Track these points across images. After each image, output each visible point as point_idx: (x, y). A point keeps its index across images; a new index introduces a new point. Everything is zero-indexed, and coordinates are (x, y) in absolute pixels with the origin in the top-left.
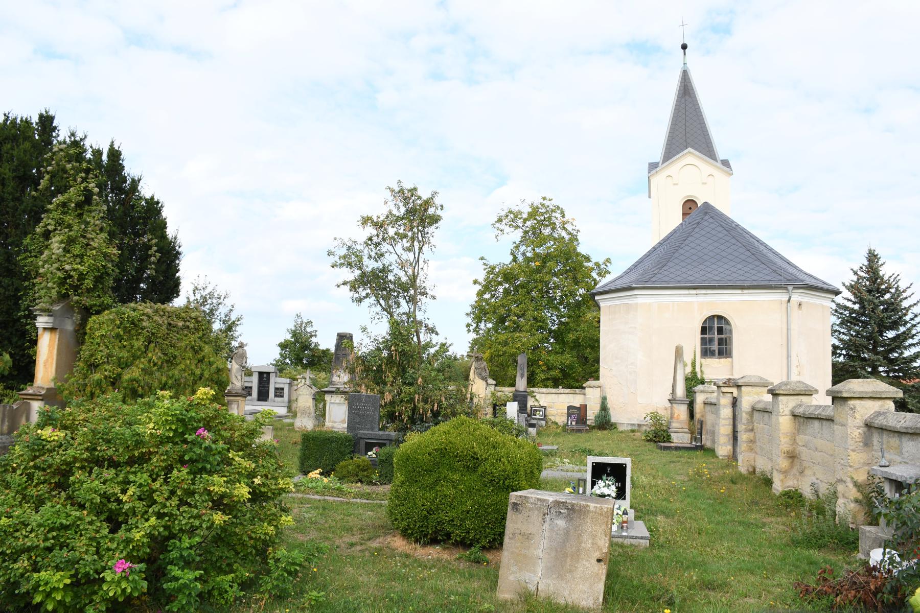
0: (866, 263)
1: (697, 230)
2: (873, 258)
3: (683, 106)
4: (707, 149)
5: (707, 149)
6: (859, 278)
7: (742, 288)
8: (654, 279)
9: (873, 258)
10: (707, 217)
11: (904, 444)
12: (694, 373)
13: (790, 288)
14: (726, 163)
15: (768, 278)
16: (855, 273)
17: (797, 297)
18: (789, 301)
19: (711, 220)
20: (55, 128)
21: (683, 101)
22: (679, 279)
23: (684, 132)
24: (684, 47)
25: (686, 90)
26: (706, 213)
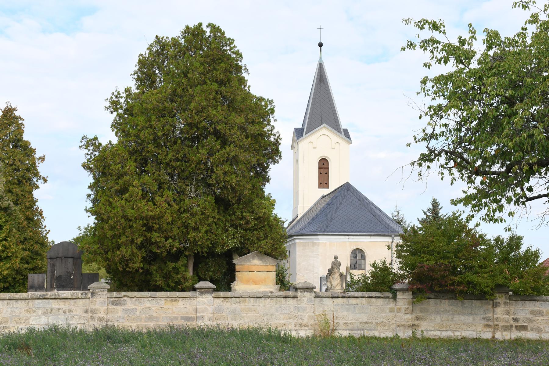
0: (431, 207)
1: (345, 200)
3: (319, 90)
4: (335, 125)
5: (334, 124)
6: (427, 216)
7: (371, 235)
8: (327, 230)
9: (435, 204)
10: (349, 192)
13: (393, 236)
14: (346, 133)
15: (383, 230)
16: (425, 213)
19: (351, 194)
21: (319, 86)
22: (340, 230)
23: (320, 111)
24: (321, 45)
25: (321, 79)
26: (348, 189)
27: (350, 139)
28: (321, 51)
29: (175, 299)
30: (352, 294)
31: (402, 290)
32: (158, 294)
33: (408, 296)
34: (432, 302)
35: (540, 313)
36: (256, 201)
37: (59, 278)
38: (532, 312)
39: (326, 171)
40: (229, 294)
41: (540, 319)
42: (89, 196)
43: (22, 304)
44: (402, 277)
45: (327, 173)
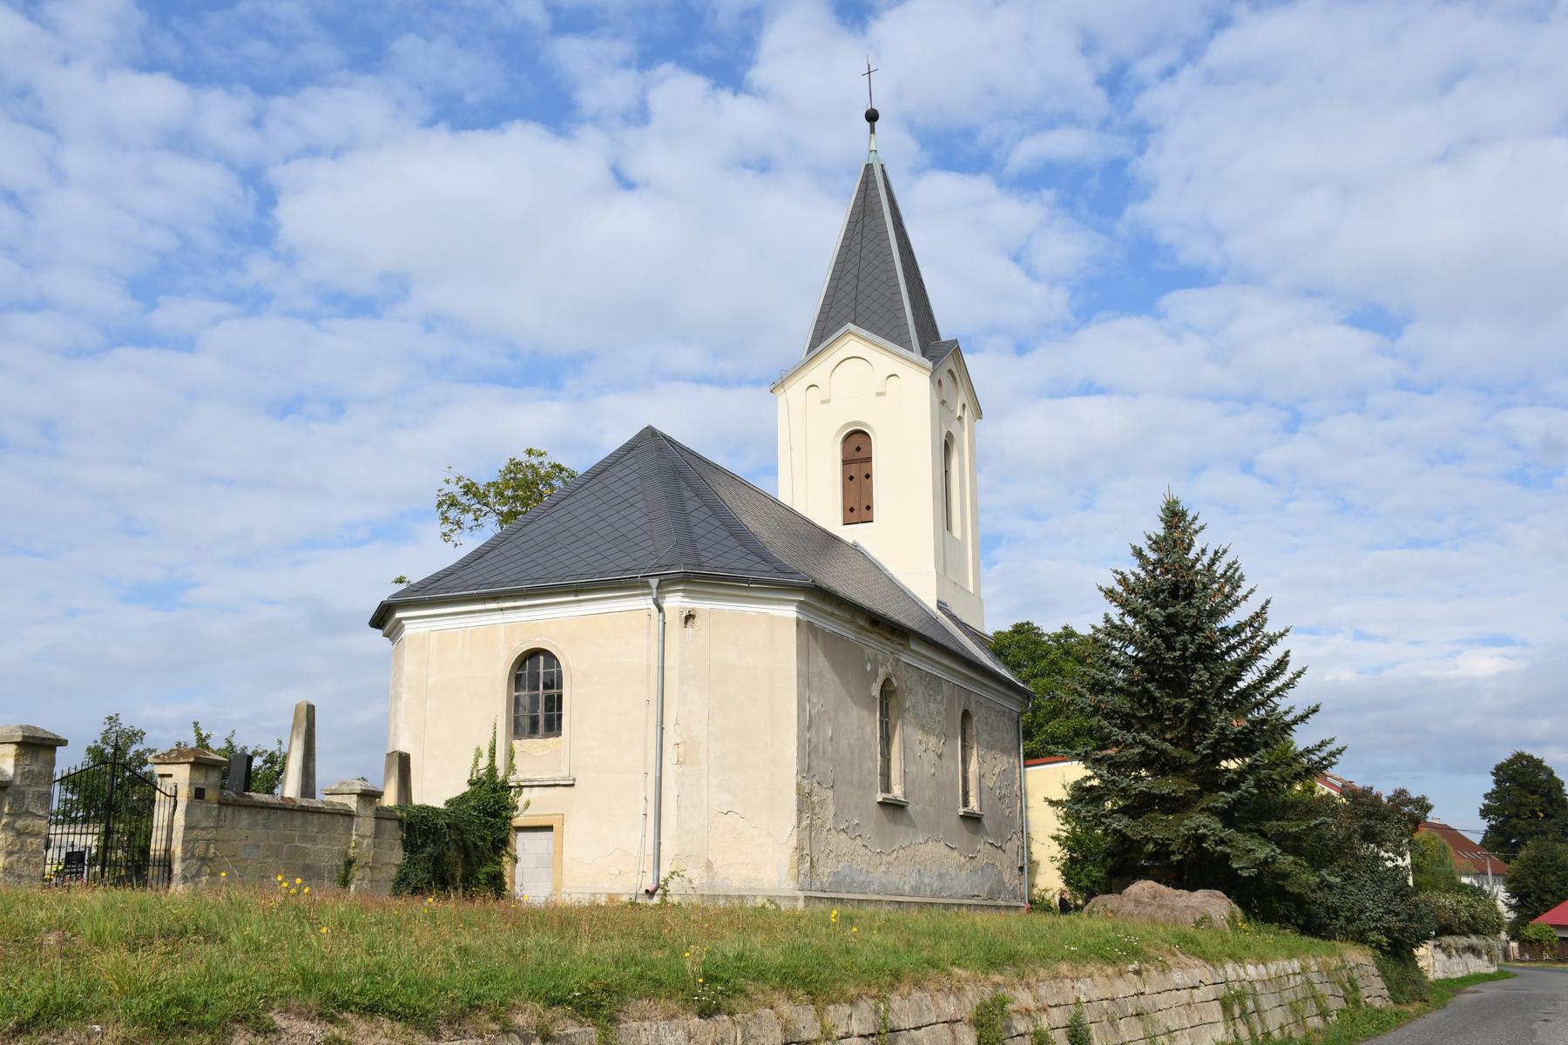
0: (1159, 529)
2: (1174, 516)
3: (857, 238)
9: (1174, 516)
11: (637, 840)
12: (492, 769)
17: (676, 602)
18: (660, 610)
20: (471, 783)
24: (872, 117)
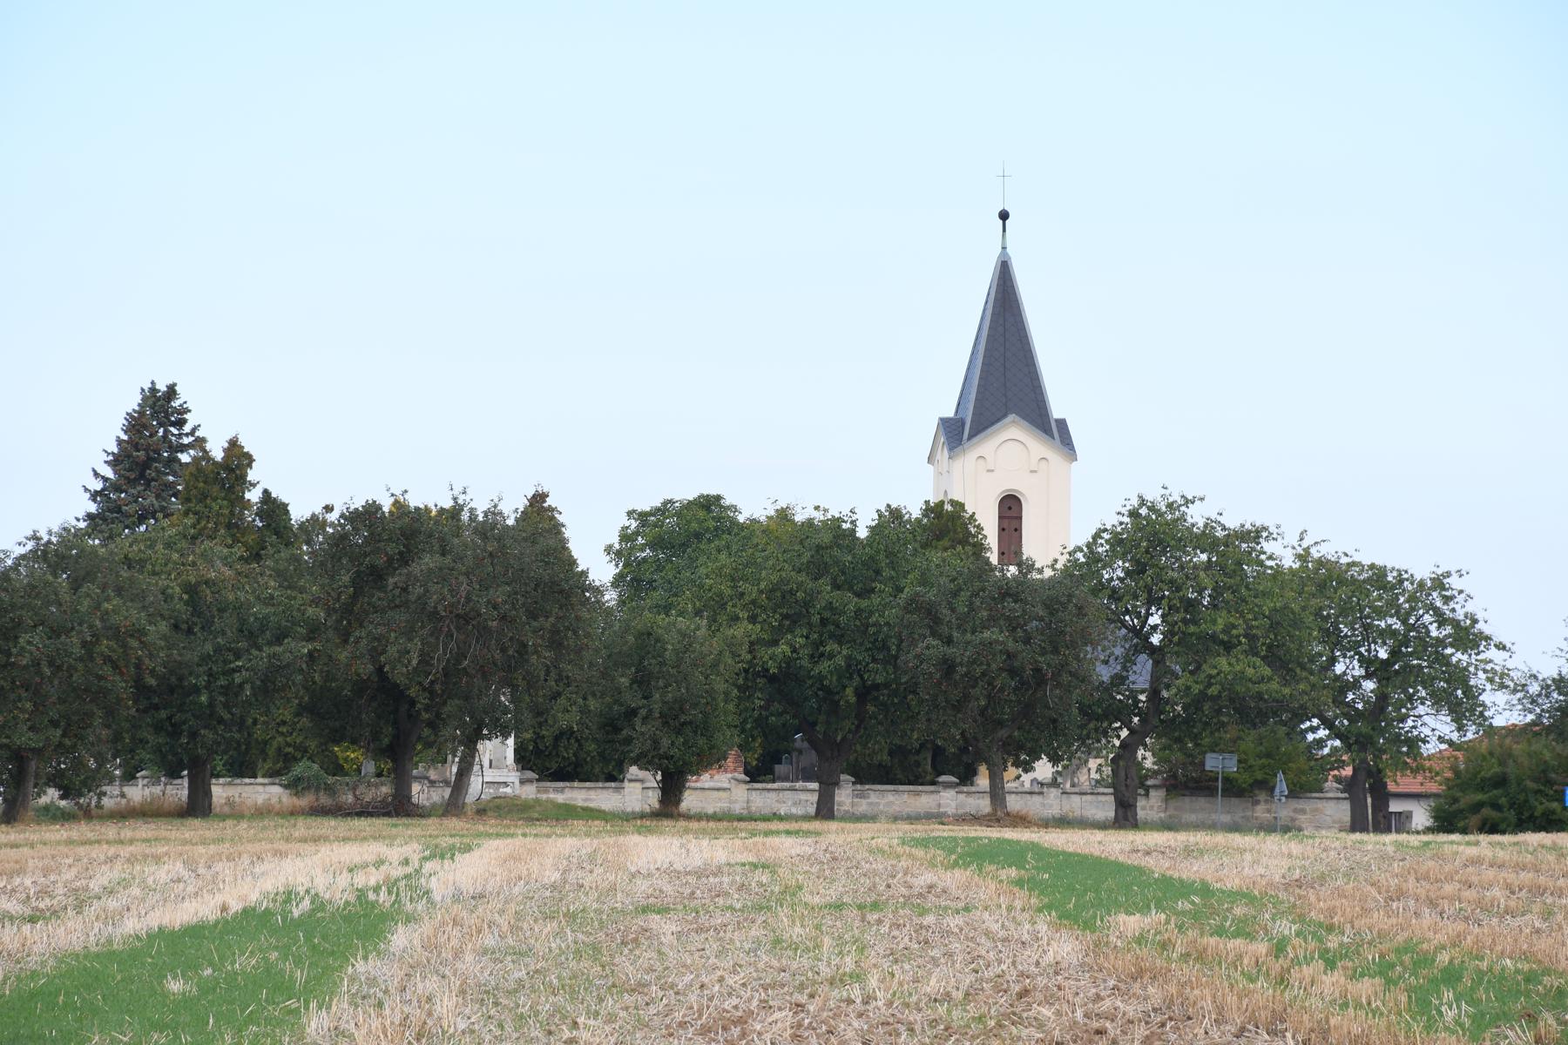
24: (1004, 216)
27: (1072, 449)
28: (1004, 248)
29: (918, 793)
30: (1102, 790)
31: (1155, 787)
32: (901, 788)
33: (1162, 793)
34: (1187, 799)
35: (1303, 811)
36: (887, 610)
37: (804, 769)
38: (1295, 811)
39: (1014, 524)
40: (973, 789)
41: (1302, 817)
42: (329, 509)
43: (773, 795)
44: (1156, 773)
45: (1018, 530)
